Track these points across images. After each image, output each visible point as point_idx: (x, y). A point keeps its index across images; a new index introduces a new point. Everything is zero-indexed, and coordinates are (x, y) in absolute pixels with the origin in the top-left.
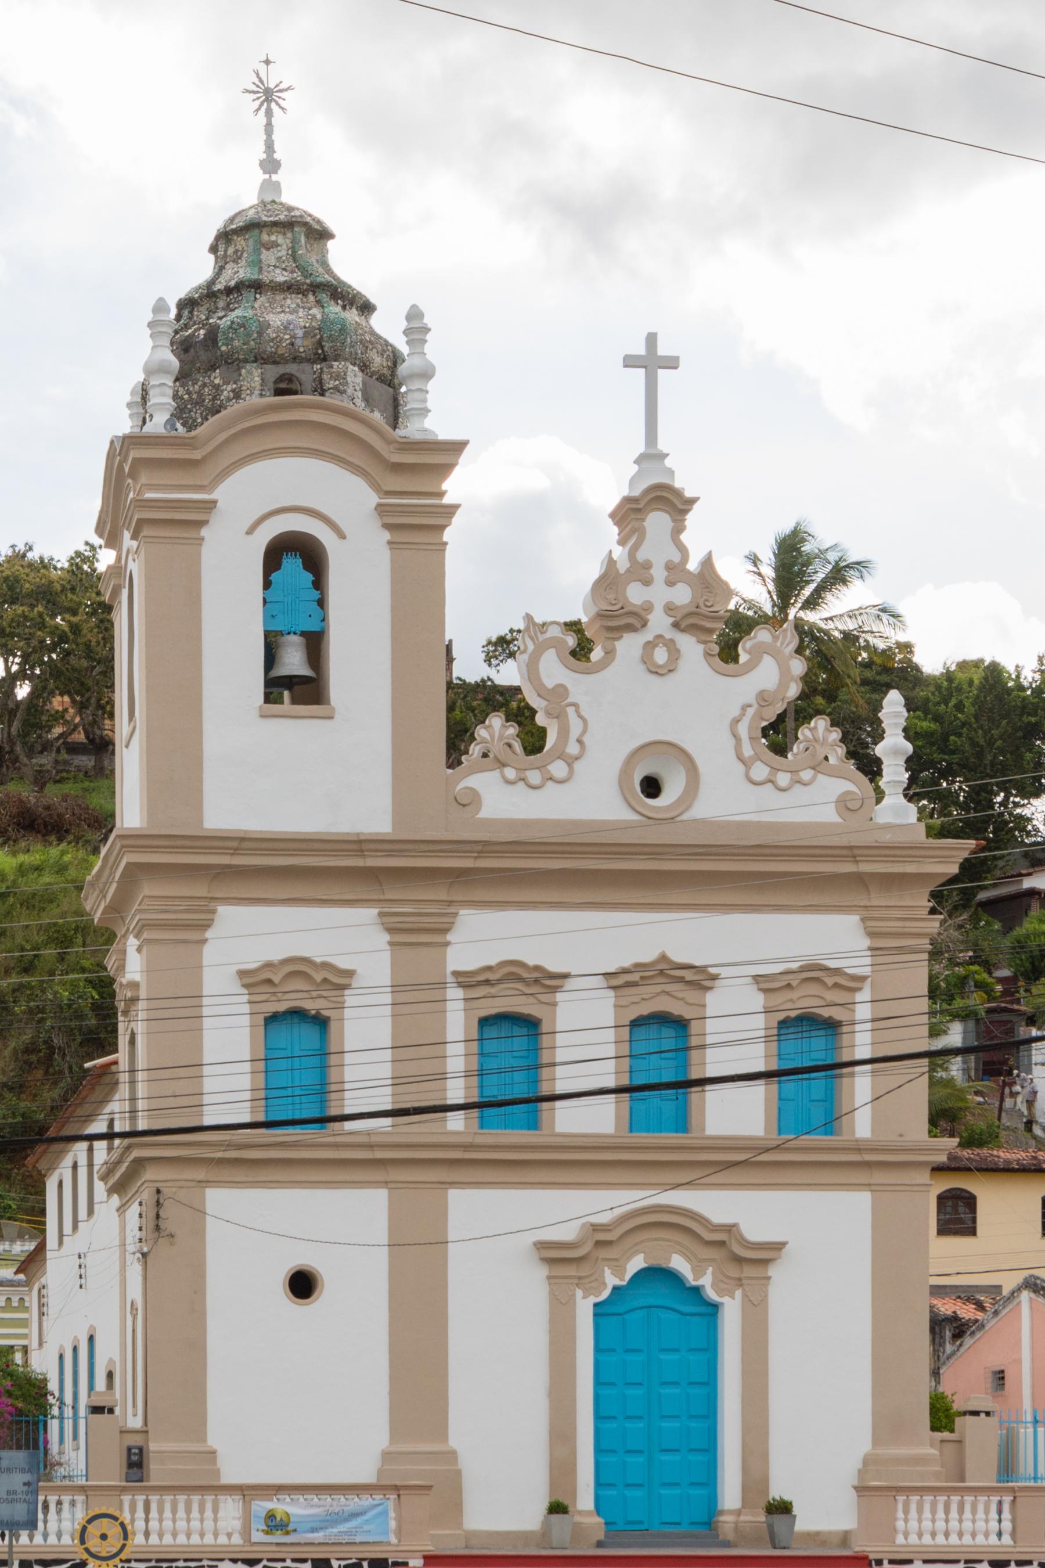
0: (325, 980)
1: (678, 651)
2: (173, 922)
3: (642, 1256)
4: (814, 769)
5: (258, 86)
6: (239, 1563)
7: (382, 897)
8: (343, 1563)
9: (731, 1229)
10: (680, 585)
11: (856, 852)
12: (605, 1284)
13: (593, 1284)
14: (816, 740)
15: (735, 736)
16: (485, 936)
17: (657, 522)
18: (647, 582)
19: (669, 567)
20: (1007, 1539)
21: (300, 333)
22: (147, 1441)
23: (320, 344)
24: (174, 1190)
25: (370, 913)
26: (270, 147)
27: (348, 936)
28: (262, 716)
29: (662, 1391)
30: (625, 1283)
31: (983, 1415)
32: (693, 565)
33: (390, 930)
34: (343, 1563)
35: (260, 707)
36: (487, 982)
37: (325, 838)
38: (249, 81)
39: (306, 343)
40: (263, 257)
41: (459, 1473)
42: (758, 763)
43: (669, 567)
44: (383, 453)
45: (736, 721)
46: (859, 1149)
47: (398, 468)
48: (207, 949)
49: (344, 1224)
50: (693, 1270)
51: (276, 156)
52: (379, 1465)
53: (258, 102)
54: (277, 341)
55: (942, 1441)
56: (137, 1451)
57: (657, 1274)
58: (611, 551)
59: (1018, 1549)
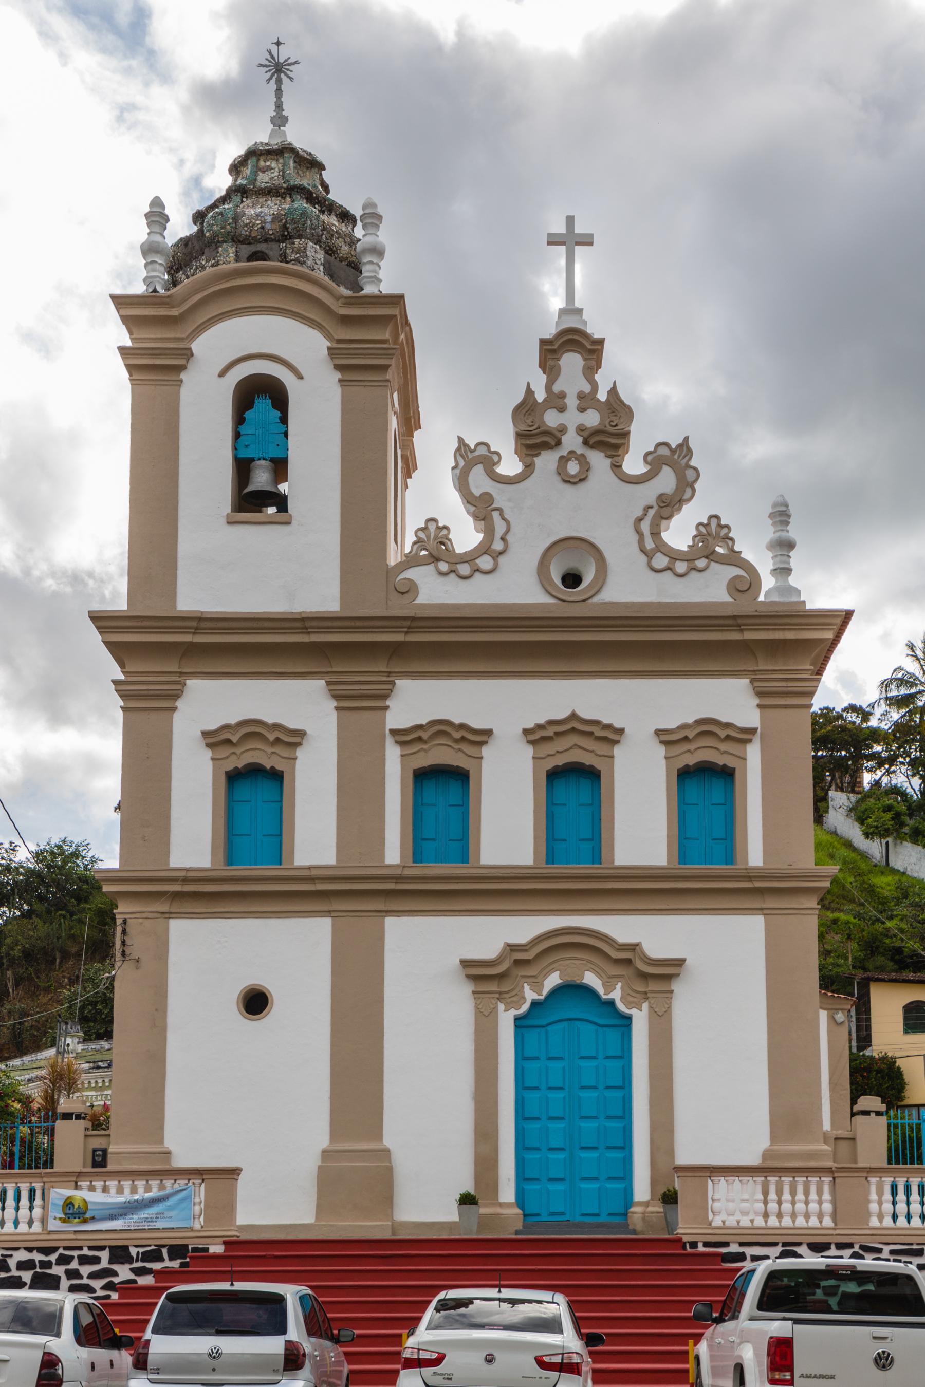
0: (278, 740)
1: (588, 463)
2: (146, 693)
3: (558, 973)
4: (707, 557)
5: (270, 61)
6: (35, 1252)
7: (330, 670)
8: (141, 1250)
9: (634, 948)
10: (590, 411)
11: (740, 621)
12: (524, 998)
13: (514, 999)
14: (709, 534)
15: (638, 532)
16: (417, 700)
17: (571, 362)
18: (562, 409)
19: (581, 396)
20: (828, 1222)
21: (269, 219)
22: (109, 1144)
23: (285, 227)
24: (140, 920)
25: (319, 684)
26: (279, 106)
27: (300, 703)
28: (228, 523)
29: (581, 1095)
30: (542, 997)
31: (873, 1115)
32: (602, 396)
33: (336, 697)
34: (141, 1250)
35: (227, 515)
36: (420, 739)
37: (272, 617)
38: (263, 58)
39: (274, 227)
40: (259, 178)
41: (390, 1170)
42: (659, 555)
43: (581, 396)
44: (332, 307)
45: (640, 520)
46: (750, 877)
47: (346, 320)
48: (177, 717)
49: (295, 952)
50: (603, 985)
51: (284, 113)
52: (320, 1163)
53: (269, 74)
54: (250, 225)
55: (836, 1139)
56: (100, 1153)
57: (573, 990)
58: (528, 384)
59: (838, 1232)
